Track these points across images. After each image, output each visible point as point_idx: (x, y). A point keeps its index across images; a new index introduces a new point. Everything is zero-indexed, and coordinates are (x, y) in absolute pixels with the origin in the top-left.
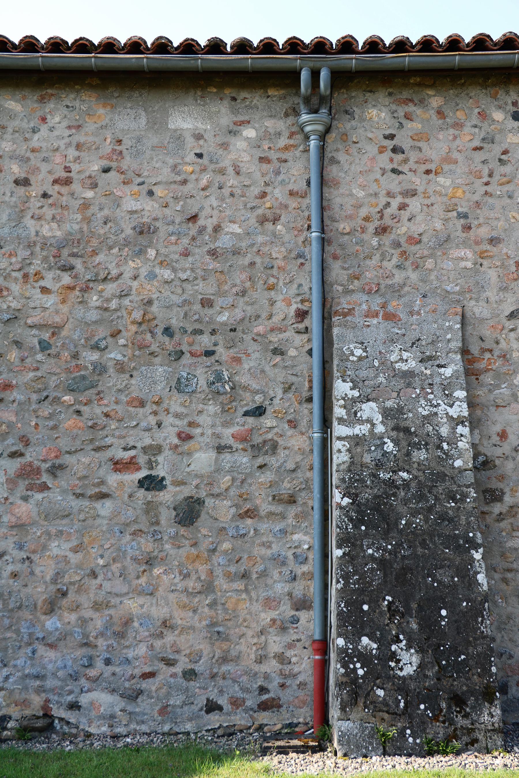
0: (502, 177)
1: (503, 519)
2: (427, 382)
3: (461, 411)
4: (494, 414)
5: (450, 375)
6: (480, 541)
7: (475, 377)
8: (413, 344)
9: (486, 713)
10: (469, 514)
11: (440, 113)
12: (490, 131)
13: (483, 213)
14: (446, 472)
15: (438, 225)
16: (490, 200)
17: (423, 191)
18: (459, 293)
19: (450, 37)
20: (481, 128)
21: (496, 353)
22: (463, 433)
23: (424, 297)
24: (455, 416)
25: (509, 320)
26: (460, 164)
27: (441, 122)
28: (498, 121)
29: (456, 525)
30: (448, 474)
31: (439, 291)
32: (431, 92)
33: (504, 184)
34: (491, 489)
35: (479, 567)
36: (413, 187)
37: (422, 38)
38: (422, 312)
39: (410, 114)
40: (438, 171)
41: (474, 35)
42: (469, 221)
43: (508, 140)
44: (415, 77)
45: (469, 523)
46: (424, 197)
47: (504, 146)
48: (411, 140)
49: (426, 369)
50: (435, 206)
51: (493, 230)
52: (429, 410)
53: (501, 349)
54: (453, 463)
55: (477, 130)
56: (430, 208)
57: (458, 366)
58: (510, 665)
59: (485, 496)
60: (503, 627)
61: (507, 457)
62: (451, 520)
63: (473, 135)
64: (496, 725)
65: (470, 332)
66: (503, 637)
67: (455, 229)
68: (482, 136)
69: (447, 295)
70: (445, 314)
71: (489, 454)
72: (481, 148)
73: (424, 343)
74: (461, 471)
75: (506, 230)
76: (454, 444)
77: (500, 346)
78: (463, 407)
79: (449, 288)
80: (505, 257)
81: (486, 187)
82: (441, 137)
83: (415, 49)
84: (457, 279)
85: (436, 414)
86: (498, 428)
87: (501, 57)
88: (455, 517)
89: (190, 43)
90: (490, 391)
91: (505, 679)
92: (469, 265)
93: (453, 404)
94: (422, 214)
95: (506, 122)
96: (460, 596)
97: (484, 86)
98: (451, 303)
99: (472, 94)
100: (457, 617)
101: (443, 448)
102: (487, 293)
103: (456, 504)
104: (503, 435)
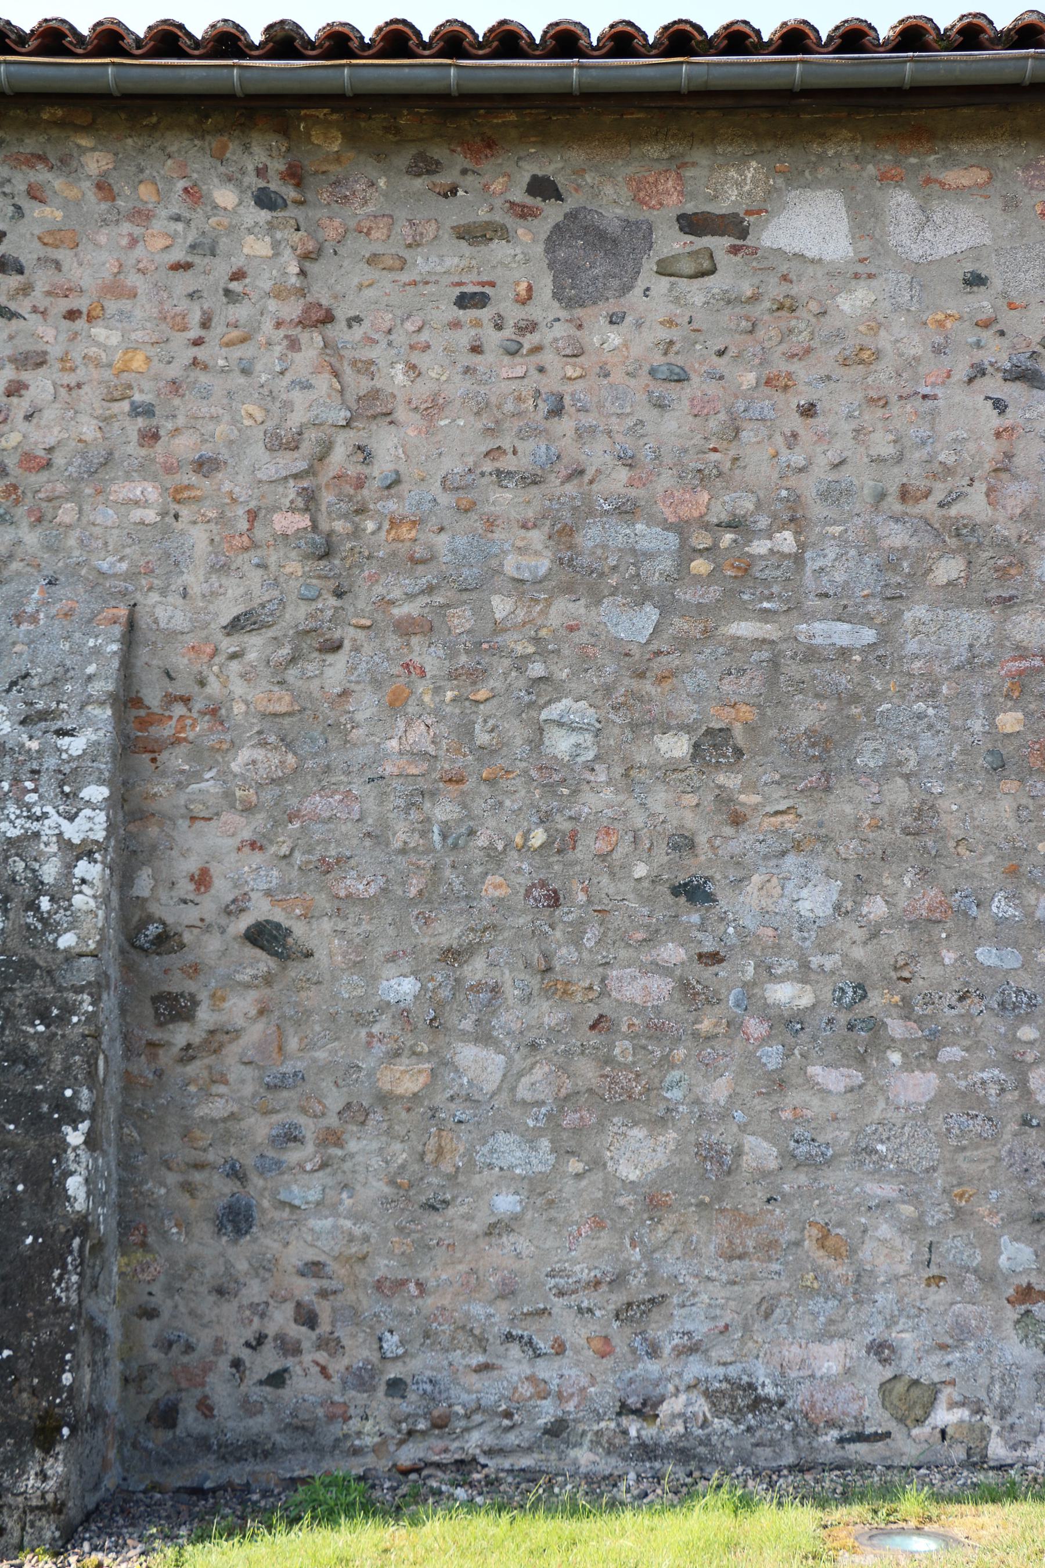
0: (230, 329)
1: (193, 1058)
2: (27, 767)
3: (91, 829)
4: (185, 834)
5: (80, 752)
6: (85, 1107)
7: (150, 756)
8: (14, 684)
9: (32, 1472)
10: (72, 1049)
11: (104, 188)
12: (207, 228)
13: (186, 406)
14: (37, 959)
15: (89, 430)
16: (204, 378)
17: (59, 355)
18: (128, 577)
19: (99, 24)
20: (188, 222)
21: (198, 705)
22: (88, 877)
23: (50, 583)
24: (76, 841)
25: (228, 635)
26: (142, 298)
27: (104, 206)
28: (225, 209)
29: (40, 1073)
30: (42, 963)
31: (83, 572)
32: (85, 142)
33: (234, 344)
34: (169, 993)
35: (75, 1161)
36: (40, 347)
37: (40, 24)
38: (42, 615)
39: (41, 187)
40: (94, 313)
41: (152, 22)
42: (154, 422)
43: (246, 250)
44: (52, 106)
45: (67, 1068)
46: (63, 369)
47: (237, 262)
48: (37, 244)
49: (31, 738)
50: (86, 388)
51: (204, 441)
52: (22, 827)
53: (209, 698)
54: (56, 940)
55: (180, 227)
56: (74, 393)
57: (101, 733)
58: (185, 1367)
59: (157, 1009)
60: (178, 1285)
61: (209, 926)
62: (30, 1062)
63: (173, 237)
64: (50, 1497)
65: (145, 659)
66: (176, 1307)
67: (124, 439)
68: (190, 240)
69: (101, 581)
70: (90, 621)
71: (170, 920)
72: (187, 266)
73: (35, 683)
74: (71, 956)
75: (232, 442)
76: (64, 899)
77: (208, 690)
78: (96, 820)
79: (105, 566)
80: (228, 501)
81: (196, 348)
82: (102, 239)
83: (27, 48)
84: (124, 547)
85: (37, 835)
86: (192, 865)
87: (203, 73)
88: (42, 1055)
89: (684, 31)
90: (179, 786)
91: (172, 1396)
92: (151, 515)
93: (76, 815)
94: (56, 405)
95: (242, 210)
96: (24, 1224)
97: (199, 132)
98: (108, 597)
99: (172, 149)
100: (8, 1268)
101: (39, 907)
102: (185, 577)
103: (47, 1026)
104: (202, 880)
